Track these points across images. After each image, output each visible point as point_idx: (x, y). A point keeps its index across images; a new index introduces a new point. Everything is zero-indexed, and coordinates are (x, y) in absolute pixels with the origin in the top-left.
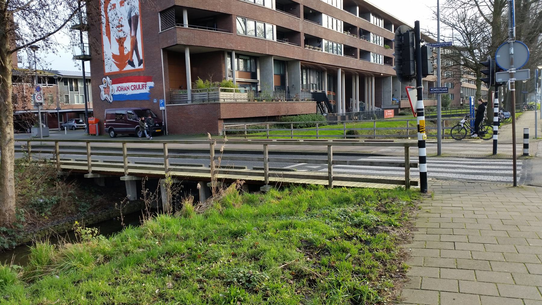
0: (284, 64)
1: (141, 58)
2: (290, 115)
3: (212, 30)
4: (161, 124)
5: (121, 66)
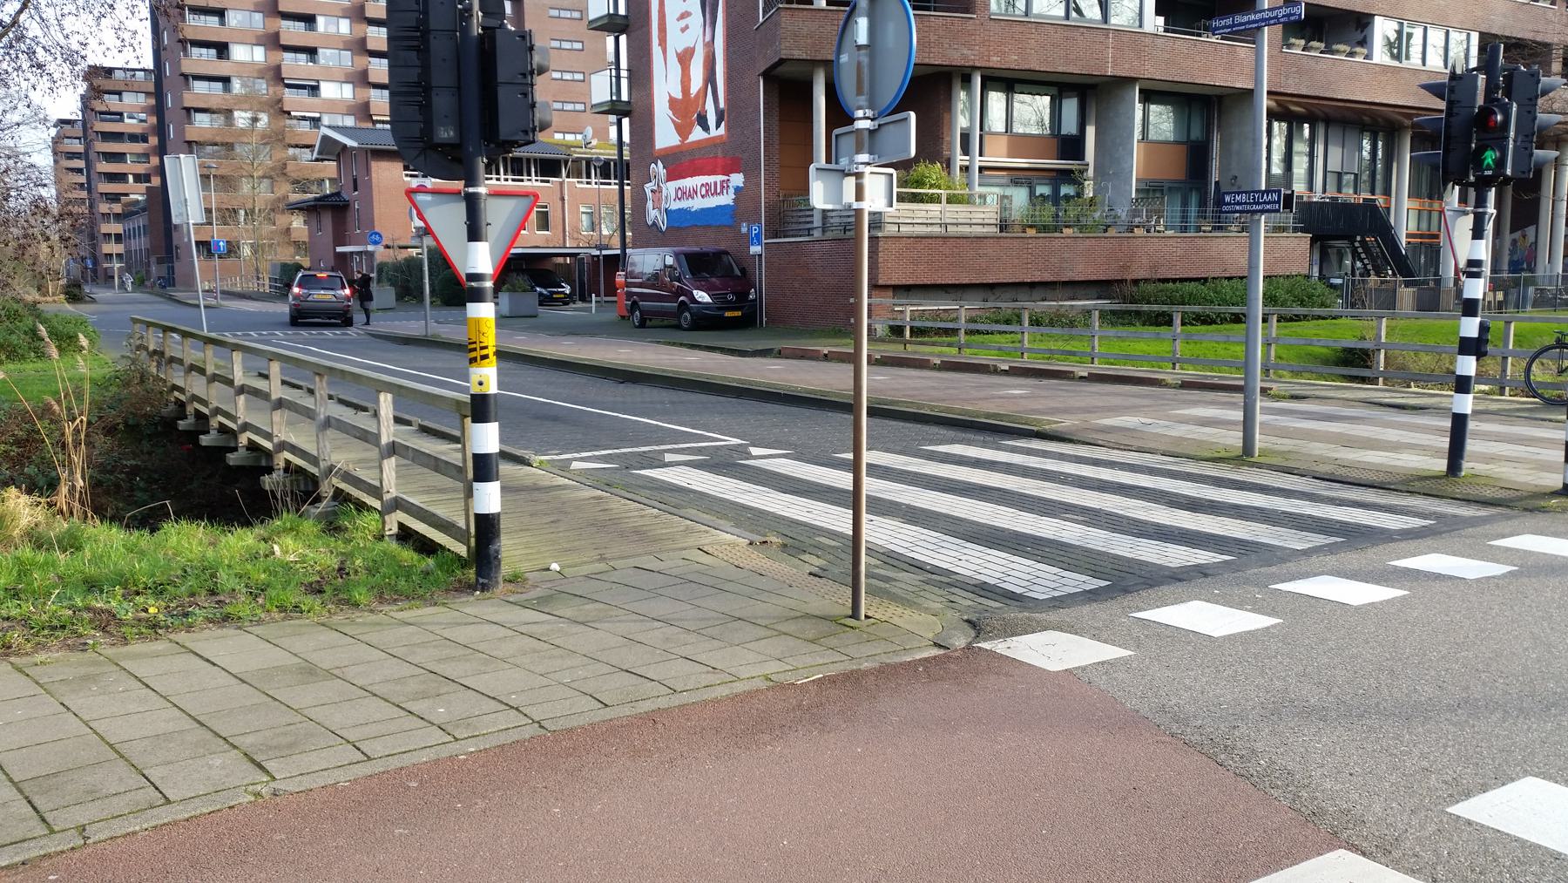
0: (1206, 108)
1: (722, 105)
2: (1182, 280)
3: (928, 9)
4: (742, 296)
5: (683, 130)
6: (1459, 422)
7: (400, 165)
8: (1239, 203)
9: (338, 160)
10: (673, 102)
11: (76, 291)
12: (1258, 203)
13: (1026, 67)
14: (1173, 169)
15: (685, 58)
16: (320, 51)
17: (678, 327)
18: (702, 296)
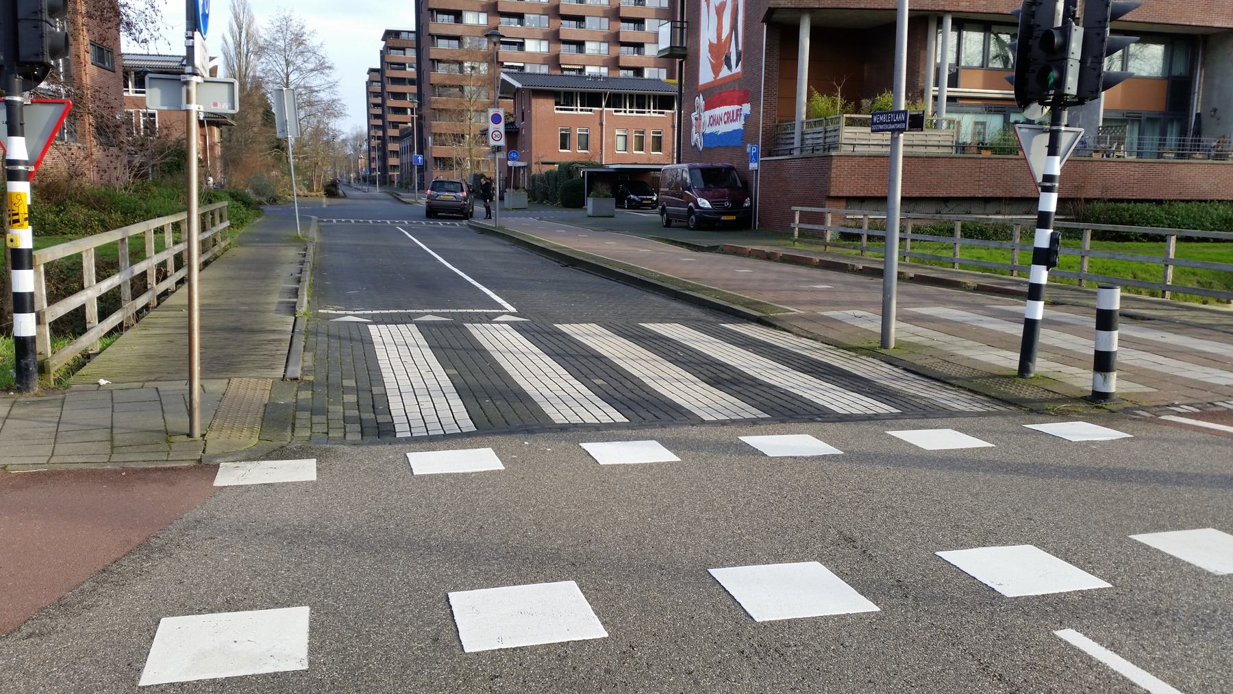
2: (1136, 201)
4: (738, 203)
5: (716, 69)
6: (1031, 326)
7: (552, 101)
8: (881, 123)
9: (514, 98)
10: (711, 45)
11: (333, 189)
12: (893, 123)
13: (994, 10)
14: (1154, 103)
15: (720, 11)
16: (587, 19)
17: (688, 228)
18: (704, 203)
